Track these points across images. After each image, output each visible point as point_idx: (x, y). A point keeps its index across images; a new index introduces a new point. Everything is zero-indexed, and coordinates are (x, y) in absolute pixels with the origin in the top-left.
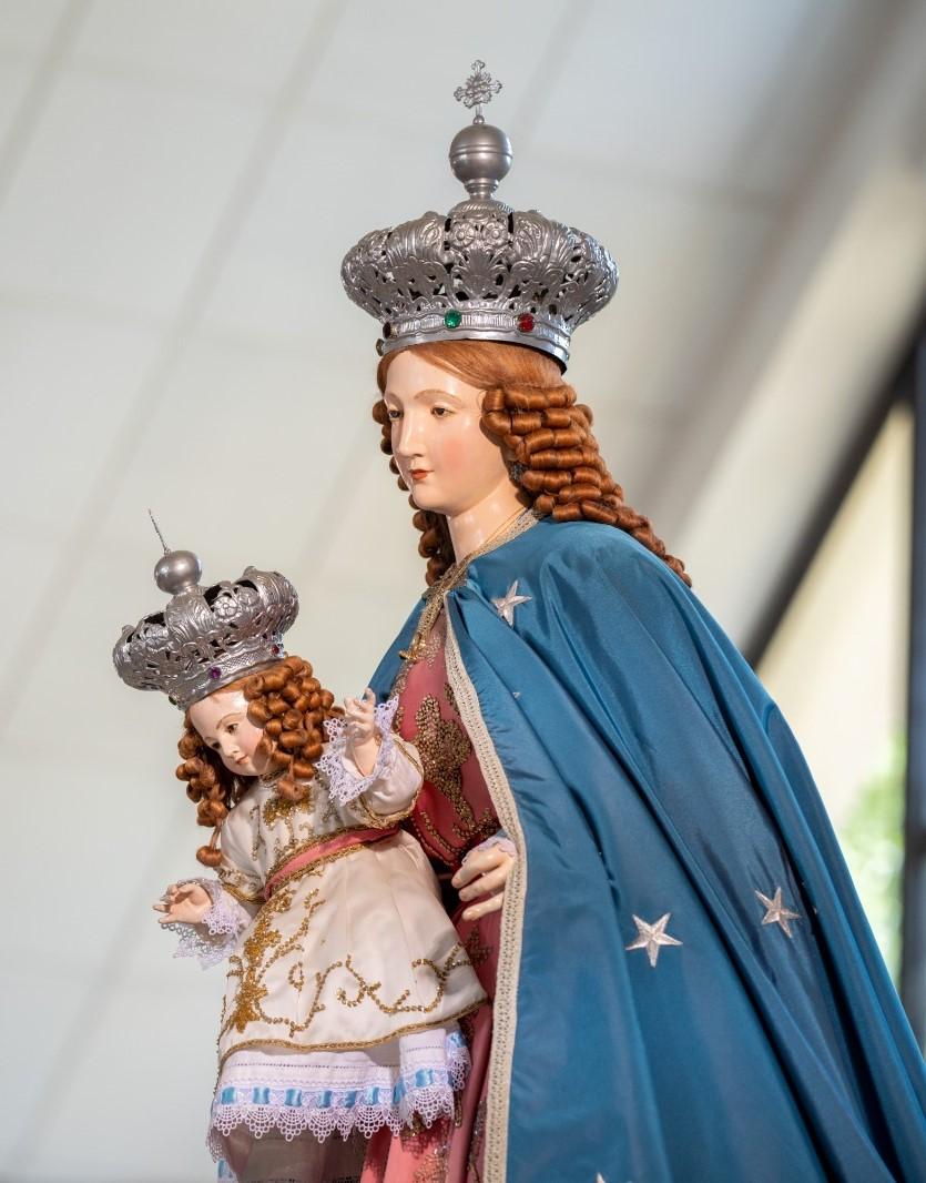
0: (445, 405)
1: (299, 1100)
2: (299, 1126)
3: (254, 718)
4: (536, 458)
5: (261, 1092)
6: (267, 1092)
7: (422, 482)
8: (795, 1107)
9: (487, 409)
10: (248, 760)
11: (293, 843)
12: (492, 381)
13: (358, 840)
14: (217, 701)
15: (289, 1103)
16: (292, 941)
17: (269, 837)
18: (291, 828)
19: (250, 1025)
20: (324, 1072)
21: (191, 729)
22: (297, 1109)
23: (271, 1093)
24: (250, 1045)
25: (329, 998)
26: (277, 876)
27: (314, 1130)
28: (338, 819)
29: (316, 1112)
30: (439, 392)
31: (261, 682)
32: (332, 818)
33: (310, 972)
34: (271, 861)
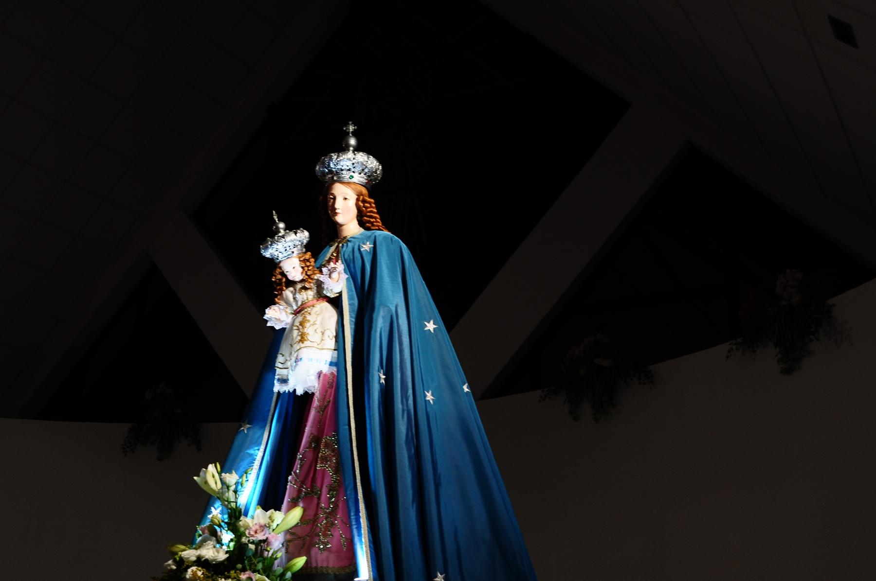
9: (358, 200)
16: (314, 322)
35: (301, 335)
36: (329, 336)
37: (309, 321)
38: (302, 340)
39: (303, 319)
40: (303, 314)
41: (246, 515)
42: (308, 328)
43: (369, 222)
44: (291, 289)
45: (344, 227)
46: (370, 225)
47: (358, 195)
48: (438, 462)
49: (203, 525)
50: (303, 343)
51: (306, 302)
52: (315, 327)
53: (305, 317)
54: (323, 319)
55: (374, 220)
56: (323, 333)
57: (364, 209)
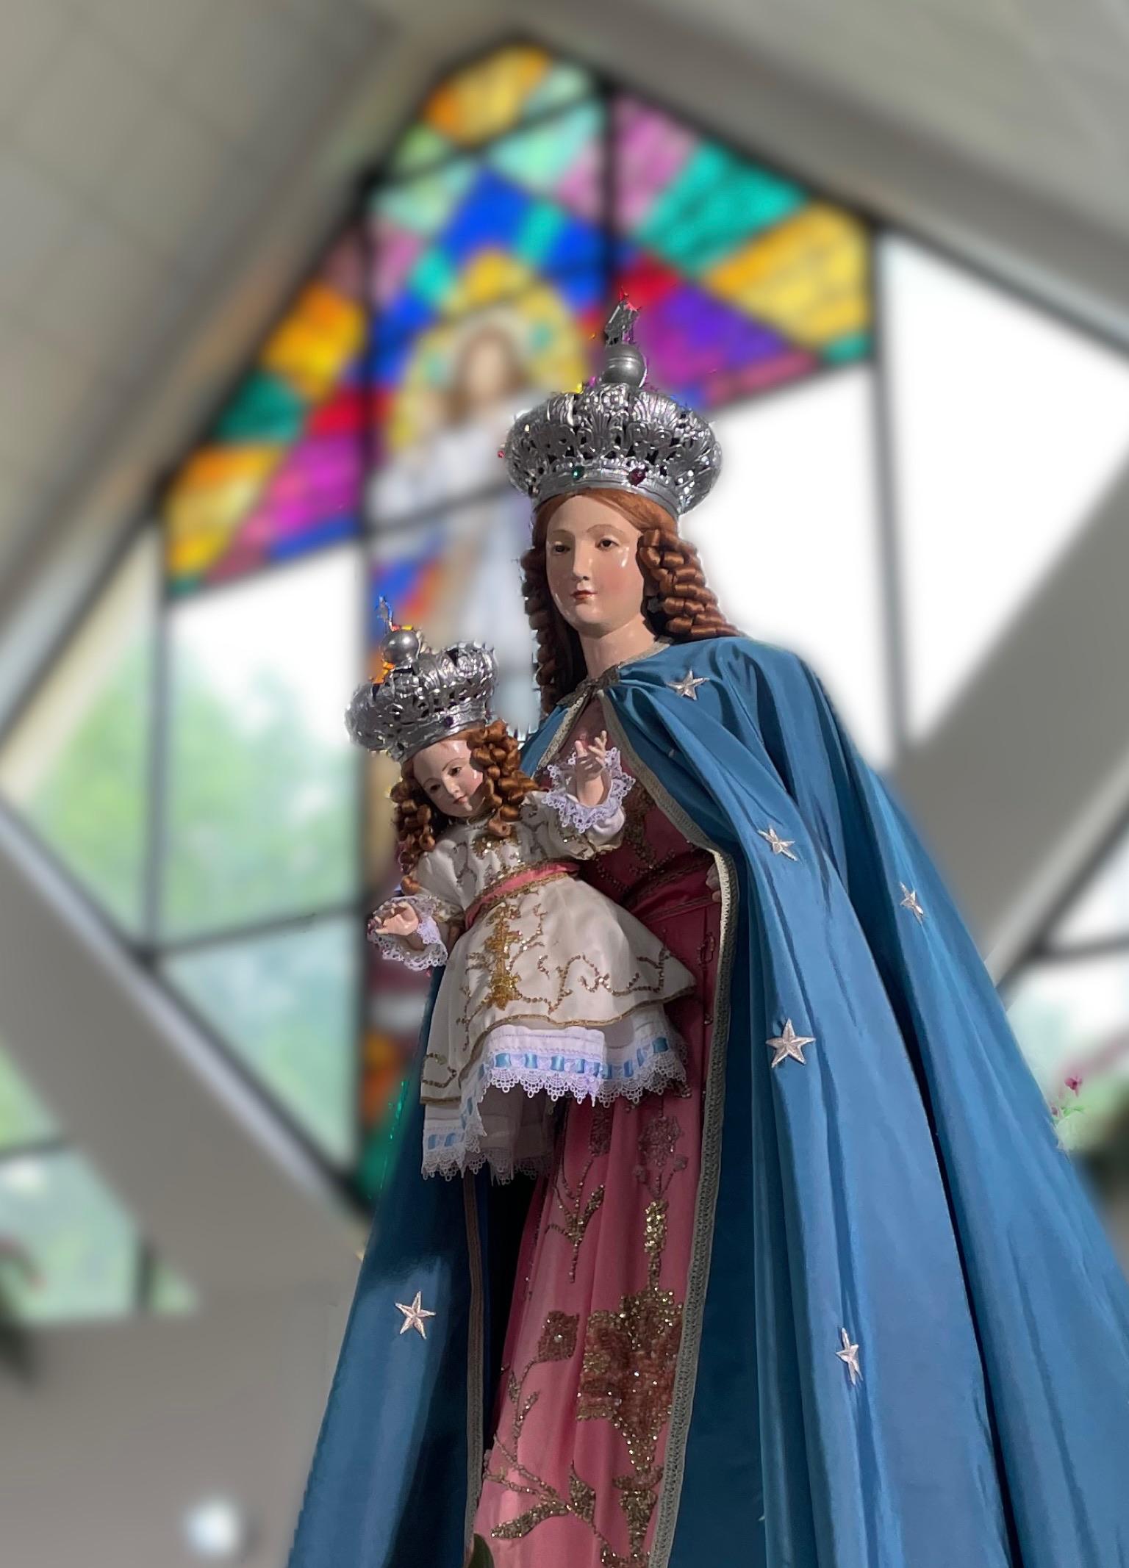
0: (612, 538)
1: (562, 1065)
2: (537, 1085)
3: (478, 764)
4: (678, 587)
5: (531, 1058)
6: (535, 1057)
7: (585, 603)
8: (927, 1073)
9: (642, 544)
10: (466, 799)
11: (505, 868)
12: (649, 523)
13: (565, 869)
14: (446, 746)
15: (553, 1068)
16: (533, 938)
17: (481, 865)
18: (501, 857)
19: (510, 1004)
20: (579, 1043)
21: (409, 774)
22: (560, 1074)
23: (538, 1059)
24: (514, 1020)
25: (575, 985)
26: (489, 896)
27: (548, 1089)
28: (543, 852)
29: (576, 1077)
30: (610, 526)
31: (486, 733)
32: (538, 851)
33: (550, 965)
34: (482, 885)
35: (494, 982)
36: (585, 982)
37: (516, 936)
38: (501, 995)
39: (496, 931)
40: (496, 915)
41: (431, 967)
42: (515, 958)
43: (683, 612)
44: (449, 843)
45: (608, 639)
46: (688, 623)
47: (642, 529)
48: (840, 1108)
49: (411, 807)
50: (502, 1007)
51: (499, 882)
52: (539, 953)
53: (501, 923)
54: (561, 924)
55: (700, 606)
56: (564, 974)
57: (664, 572)
